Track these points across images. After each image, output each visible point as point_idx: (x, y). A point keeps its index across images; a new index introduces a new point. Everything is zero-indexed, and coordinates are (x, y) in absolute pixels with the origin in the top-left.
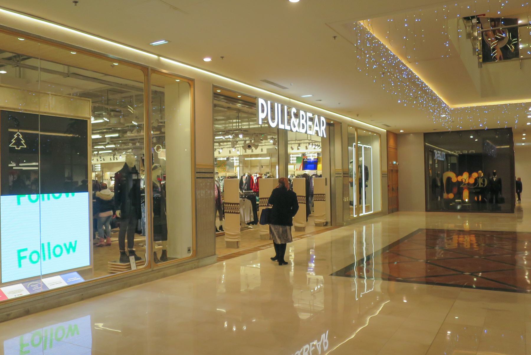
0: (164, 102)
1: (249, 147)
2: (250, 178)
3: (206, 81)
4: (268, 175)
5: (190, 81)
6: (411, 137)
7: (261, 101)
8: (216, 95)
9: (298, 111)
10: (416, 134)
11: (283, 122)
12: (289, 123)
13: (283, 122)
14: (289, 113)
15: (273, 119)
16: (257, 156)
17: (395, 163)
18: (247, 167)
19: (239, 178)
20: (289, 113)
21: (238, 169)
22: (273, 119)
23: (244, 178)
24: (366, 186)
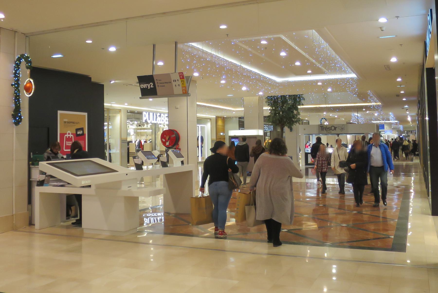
0: (32, 33)
1: (140, 126)
2: (140, 142)
3: (125, 109)
4: (151, 140)
5: (120, 111)
6: (234, 119)
7: (144, 113)
8: (128, 112)
9: (160, 114)
10: (236, 117)
11: (153, 120)
12: (156, 120)
13: (153, 120)
14: (156, 115)
15: (149, 119)
16: (144, 129)
17: (222, 134)
18: (138, 135)
19: (133, 142)
20: (156, 115)
21: (133, 137)
22: (149, 119)
23: (137, 142)
24: (202, 147)
